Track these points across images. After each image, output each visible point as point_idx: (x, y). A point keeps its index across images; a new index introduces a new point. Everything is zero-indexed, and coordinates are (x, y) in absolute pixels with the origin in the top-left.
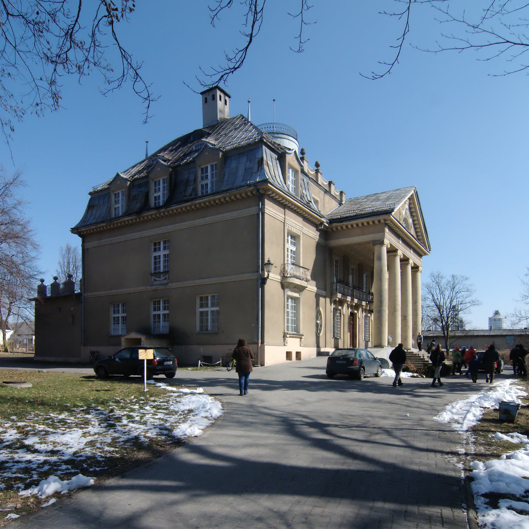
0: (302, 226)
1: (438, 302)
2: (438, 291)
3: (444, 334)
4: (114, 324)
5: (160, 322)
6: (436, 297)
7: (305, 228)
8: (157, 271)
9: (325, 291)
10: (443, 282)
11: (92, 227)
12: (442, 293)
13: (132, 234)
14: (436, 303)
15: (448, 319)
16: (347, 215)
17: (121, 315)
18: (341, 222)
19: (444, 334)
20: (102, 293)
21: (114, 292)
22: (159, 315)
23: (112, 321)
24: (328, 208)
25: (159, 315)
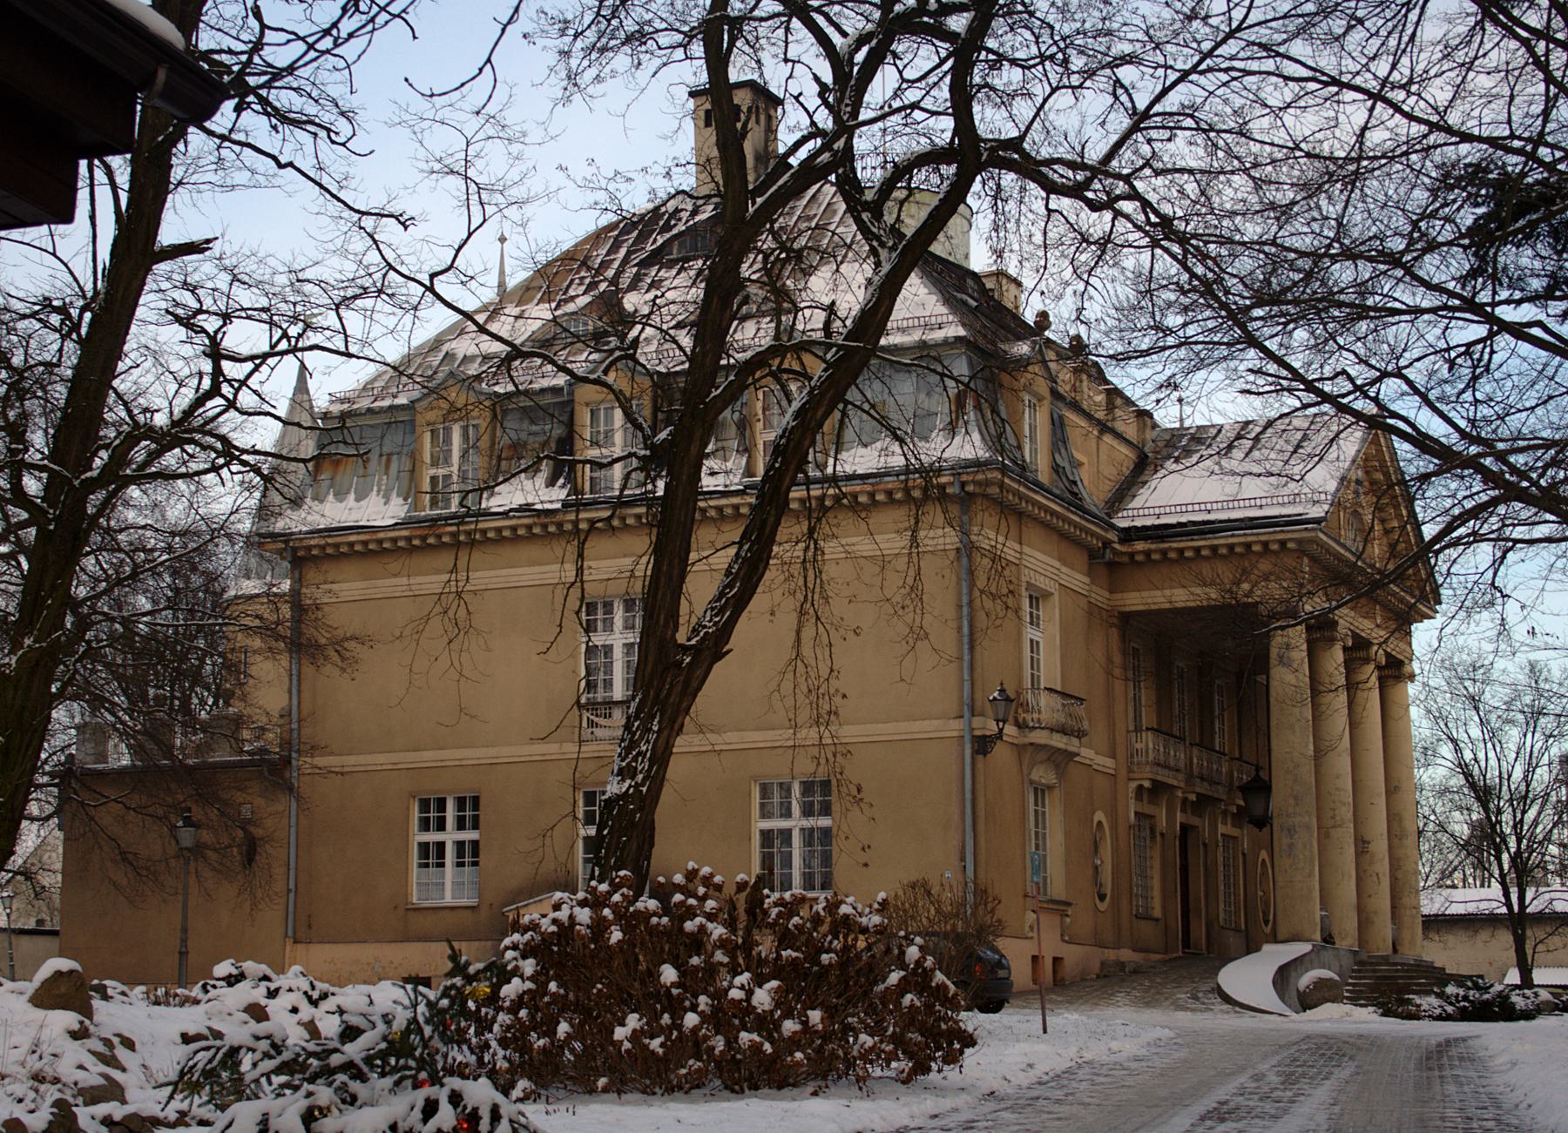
0: (1057, 564)
1: (1476, 772)
2: (1475, 732)
3: (1508, 904)
4: (460, 865)
5: (442, 865)
6: (1468, 755)
7: (1064, 569)
8: (600, 695)
9: (1114, 757)
10: (1494, 697)
11: (352, 538)
12: (1493, 736)
13: (505, 572)
14: (1468, 775)
15: (1519, 842)
16: (1183, 519)
17: (450, 836)
18: (1162, 539)
19: (1508, 904)
20: (381, 759)
21: (428, 757)
22: (441, 846)
23: (415, 858)
24: (1004, 112)
25: (441, 846)
